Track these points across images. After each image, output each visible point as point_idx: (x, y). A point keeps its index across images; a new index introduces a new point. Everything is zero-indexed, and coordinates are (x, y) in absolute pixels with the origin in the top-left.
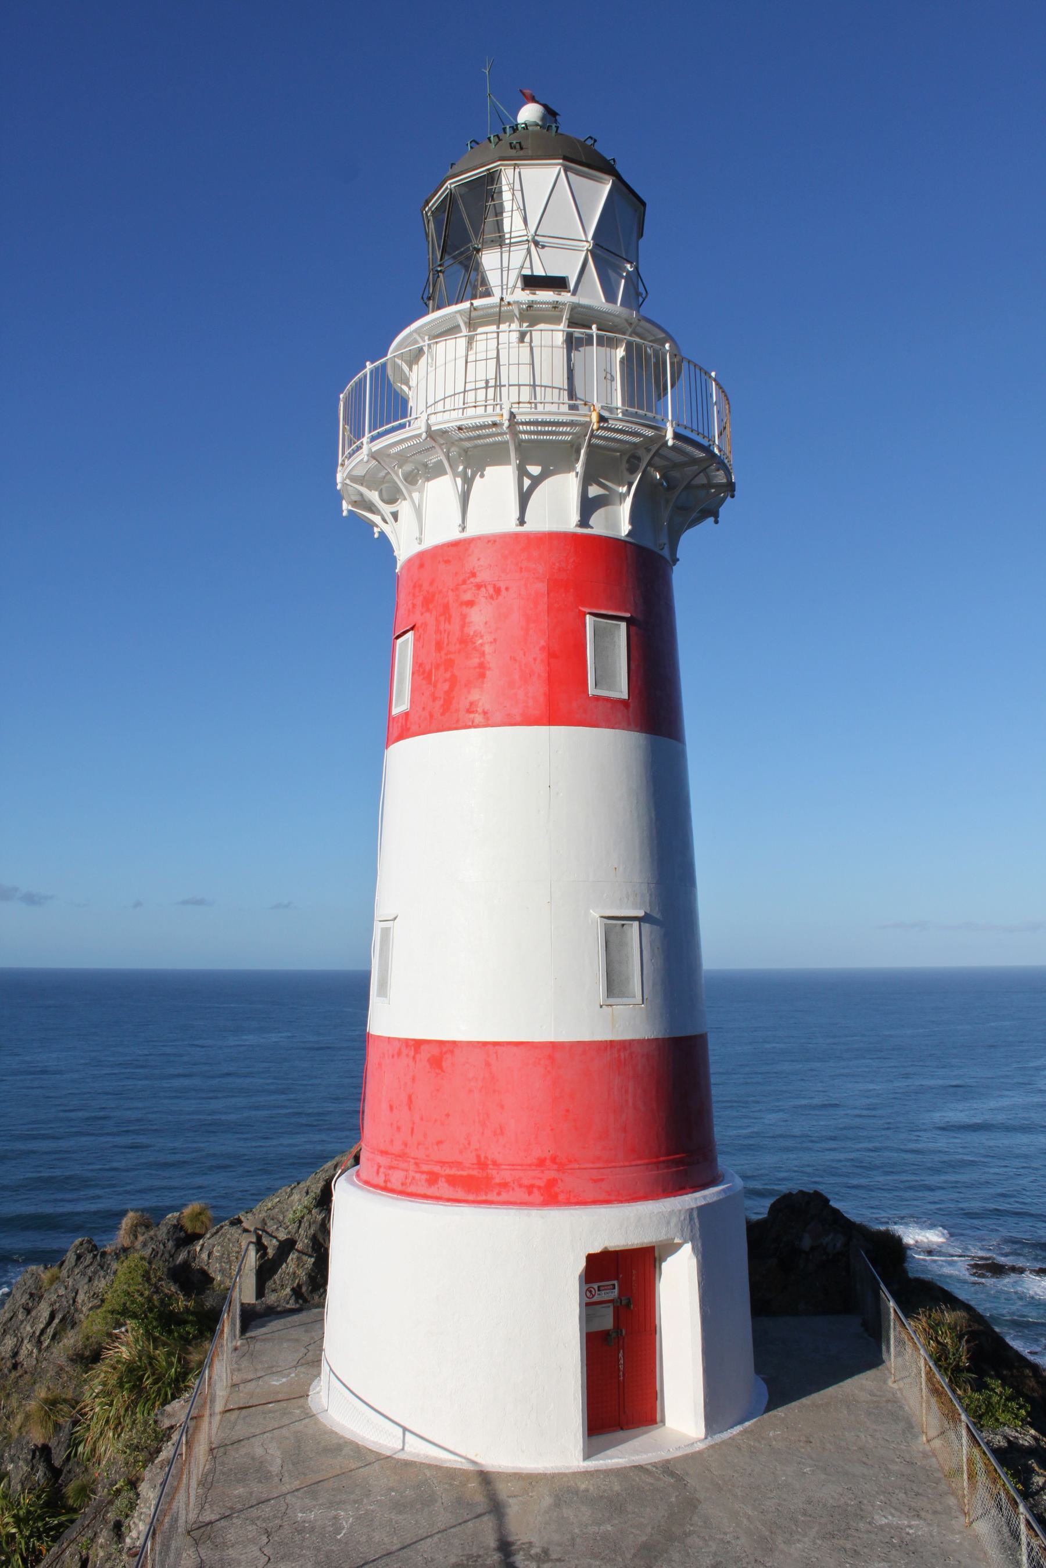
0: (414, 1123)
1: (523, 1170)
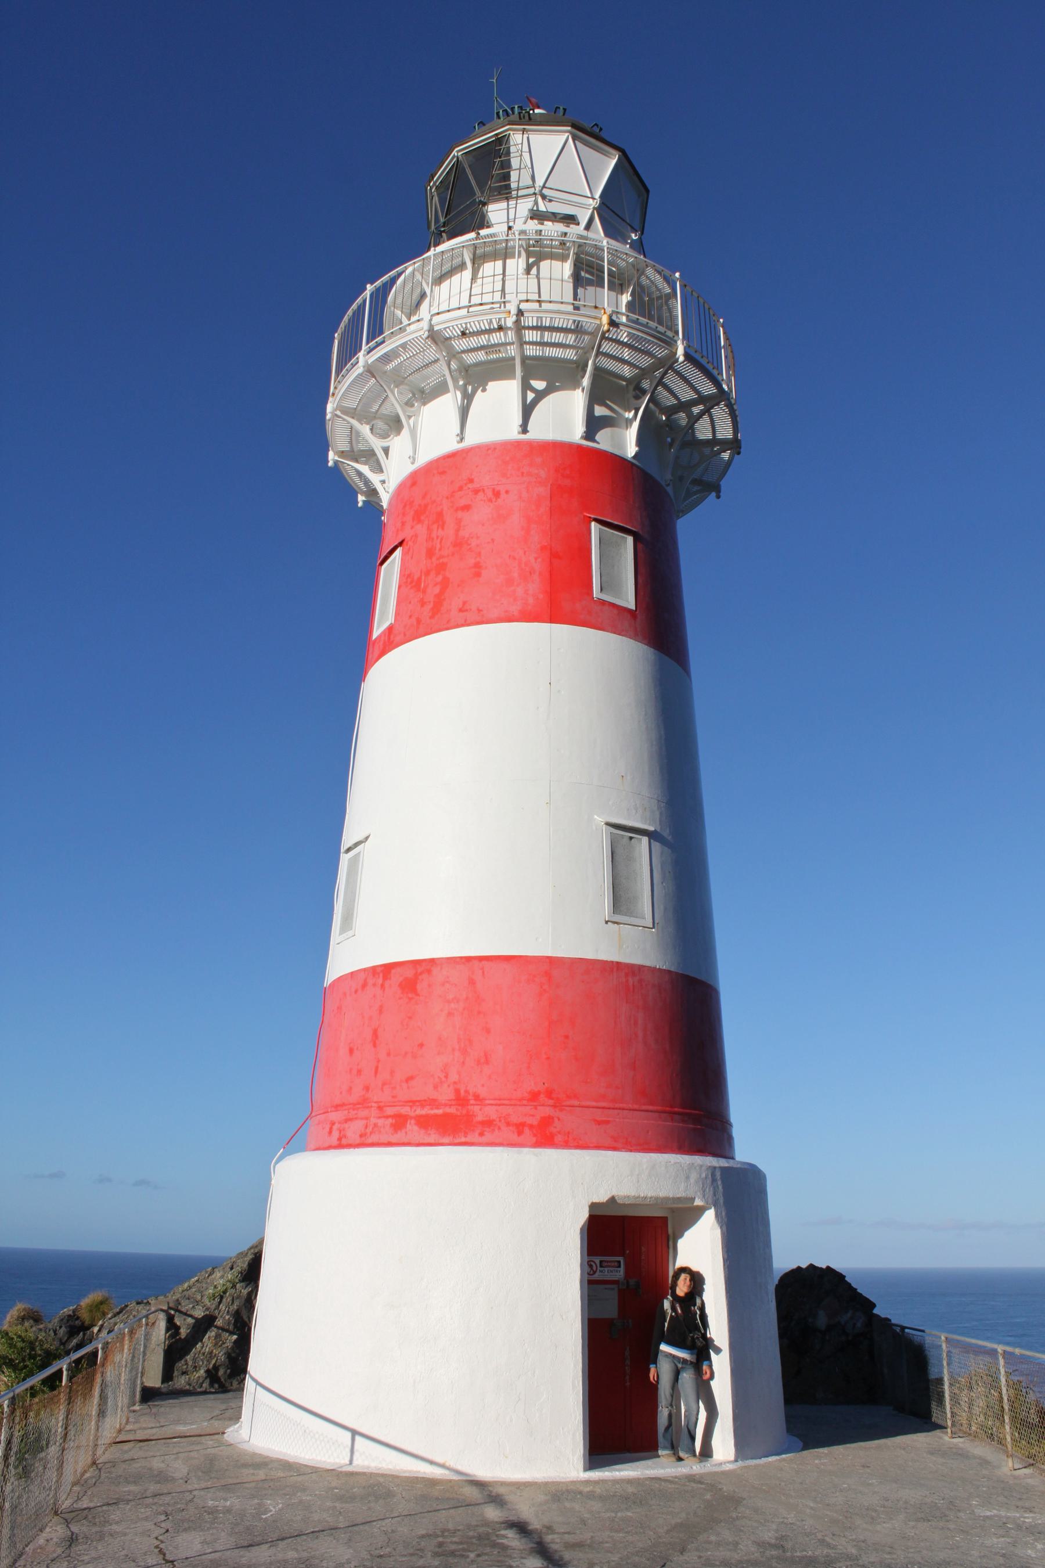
0: (378, 1061)
1: (511, 1105)
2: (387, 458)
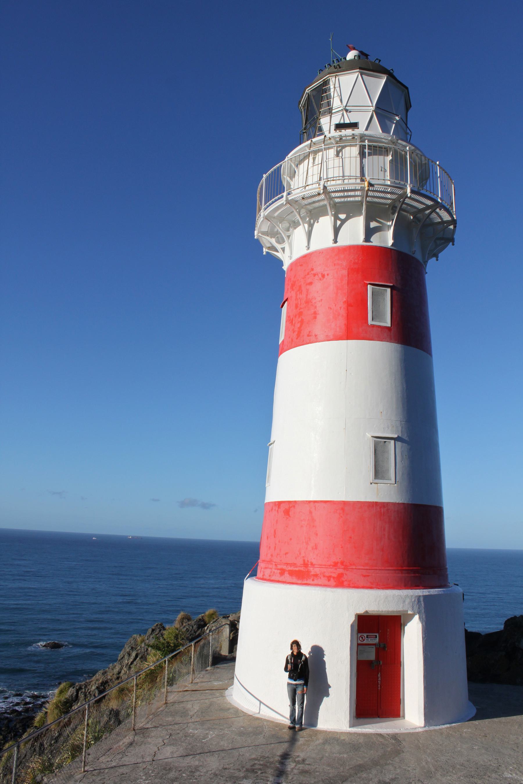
0: (276, 544)
2: (284, 253)
